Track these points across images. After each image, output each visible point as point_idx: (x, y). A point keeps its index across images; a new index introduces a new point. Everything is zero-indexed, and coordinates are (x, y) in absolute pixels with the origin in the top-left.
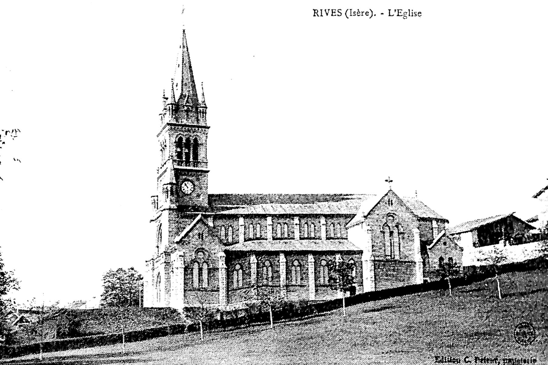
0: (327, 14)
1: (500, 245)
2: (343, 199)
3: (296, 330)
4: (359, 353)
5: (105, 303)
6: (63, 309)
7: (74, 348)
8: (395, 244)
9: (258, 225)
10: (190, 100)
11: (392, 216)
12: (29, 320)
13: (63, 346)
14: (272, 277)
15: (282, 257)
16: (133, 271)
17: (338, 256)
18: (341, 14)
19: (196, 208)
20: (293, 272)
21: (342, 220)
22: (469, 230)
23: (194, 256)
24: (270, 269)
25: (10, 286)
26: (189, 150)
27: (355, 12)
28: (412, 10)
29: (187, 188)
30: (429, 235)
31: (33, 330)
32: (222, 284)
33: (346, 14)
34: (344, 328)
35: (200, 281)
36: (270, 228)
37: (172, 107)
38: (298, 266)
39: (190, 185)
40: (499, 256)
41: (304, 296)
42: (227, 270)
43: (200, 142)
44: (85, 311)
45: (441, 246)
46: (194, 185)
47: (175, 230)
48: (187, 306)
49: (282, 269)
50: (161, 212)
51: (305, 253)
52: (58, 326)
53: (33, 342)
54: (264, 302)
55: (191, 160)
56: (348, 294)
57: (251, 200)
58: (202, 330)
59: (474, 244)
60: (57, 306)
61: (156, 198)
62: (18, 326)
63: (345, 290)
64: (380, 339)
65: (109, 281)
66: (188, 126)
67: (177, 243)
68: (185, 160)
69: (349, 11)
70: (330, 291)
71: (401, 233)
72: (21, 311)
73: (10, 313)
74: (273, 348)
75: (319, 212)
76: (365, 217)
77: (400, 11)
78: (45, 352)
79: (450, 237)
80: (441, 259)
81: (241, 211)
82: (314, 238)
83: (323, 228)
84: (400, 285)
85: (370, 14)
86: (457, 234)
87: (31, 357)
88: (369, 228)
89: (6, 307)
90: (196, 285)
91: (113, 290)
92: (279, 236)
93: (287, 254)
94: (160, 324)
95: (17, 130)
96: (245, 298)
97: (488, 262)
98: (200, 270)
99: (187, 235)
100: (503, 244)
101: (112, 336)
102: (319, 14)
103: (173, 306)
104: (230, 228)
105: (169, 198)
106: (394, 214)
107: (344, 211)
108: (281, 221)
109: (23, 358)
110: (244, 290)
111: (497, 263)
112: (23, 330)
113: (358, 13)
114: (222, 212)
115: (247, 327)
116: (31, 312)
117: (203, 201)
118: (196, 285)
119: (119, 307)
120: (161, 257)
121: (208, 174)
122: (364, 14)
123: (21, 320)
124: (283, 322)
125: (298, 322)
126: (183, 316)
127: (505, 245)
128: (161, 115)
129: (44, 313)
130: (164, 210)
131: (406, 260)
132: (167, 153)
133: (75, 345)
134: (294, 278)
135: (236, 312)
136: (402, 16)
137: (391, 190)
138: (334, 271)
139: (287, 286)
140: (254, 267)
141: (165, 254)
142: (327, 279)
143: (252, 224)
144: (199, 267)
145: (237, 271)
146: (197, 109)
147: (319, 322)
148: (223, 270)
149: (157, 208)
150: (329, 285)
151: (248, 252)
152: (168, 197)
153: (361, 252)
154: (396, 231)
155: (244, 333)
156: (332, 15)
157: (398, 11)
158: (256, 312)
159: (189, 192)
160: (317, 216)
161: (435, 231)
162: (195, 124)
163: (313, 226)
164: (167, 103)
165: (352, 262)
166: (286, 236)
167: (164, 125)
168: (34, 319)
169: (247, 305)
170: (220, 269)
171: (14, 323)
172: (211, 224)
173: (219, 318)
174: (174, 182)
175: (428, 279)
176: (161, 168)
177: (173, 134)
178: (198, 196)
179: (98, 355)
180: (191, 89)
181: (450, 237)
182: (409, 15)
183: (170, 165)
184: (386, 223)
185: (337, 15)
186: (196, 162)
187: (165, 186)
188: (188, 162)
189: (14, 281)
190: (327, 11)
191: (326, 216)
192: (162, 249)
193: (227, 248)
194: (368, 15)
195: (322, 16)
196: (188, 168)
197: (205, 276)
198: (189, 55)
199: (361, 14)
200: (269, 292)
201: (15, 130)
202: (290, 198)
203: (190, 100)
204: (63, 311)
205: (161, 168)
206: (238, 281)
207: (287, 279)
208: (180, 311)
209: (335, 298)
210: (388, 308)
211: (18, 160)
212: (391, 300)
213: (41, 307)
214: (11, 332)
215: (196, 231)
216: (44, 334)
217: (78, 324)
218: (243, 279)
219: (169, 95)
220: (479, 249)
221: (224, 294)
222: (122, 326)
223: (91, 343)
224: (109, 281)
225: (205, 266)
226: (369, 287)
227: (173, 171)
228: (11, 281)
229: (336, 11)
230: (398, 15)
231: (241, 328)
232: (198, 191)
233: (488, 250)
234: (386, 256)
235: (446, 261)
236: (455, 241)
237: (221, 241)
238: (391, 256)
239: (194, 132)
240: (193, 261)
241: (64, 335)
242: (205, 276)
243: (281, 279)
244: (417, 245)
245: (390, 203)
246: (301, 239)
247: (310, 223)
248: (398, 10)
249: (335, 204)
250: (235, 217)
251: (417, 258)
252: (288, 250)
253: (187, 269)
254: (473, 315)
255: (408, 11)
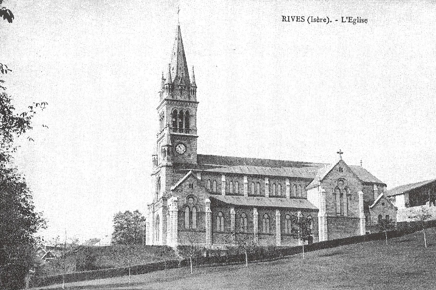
0: (293, 20)
1: (427, 206)
2: (303, 166)
3: (265, 269)
4: (315, 287)
5: (115, 241)
6: (81, 246)
7: (90, 279)
8: (345, 204)
9: (237, 183)
10: (183, 81)
11: (342, 181)
12: (54, 255)
13: (82, 278)
14: (247, 227)
15: (255, 212)
16: (138, 213)
17: (299, 213)
18: (304, 20)
19: (188, 166)
20: (264, 224)
21: (303, 183)
22: (402, 193)
23: (185, 201)
24: (246, 219)
25: (40, 226)
26: (182, 120)
27: (315, 19)
28: (360, 18)
29: (181, 149)
30: (371, 197)
31: (58, 264)
32: (207, 225)
33: (308, 20)
34: (303, 268)
35: (191, 223)
36: (246, 186)
37: (169, 87)
38: (268, 218)
39: (182, 147)
40: (425, 214)
41: (272, 243)
42: (212, 214)
43: (190, 114)
44: (99, 248)
45: (380, 206)
46: (186, 147)
47: (171, 182)
48: (180, 244)
49: (255, 221)
50: (160, 169)
51: (273, 209)
52: (77, 260)
53: (57, 274)
54: (240, 246)
55: (184, 128)
56: (307, 242)
57: (231, 162)
58: (191, 265)
59: (406, 205)
60: (76, 243)
61: (156, 157)
62: (45, 260)
63: (304, 240)
64: (332, 277)
65: (119, 222)
66: (181, 101)
67: (172, 190)
68: (179, 128)
69: (310, 18)
70: (292, 240)
71: (349, 195)
72: (48, 248)
73: (39, 249)
74: (248, 282)
75: (284, 175)
76: (320, 181)
77: (351, 18)
78: (68, 282)
79: (387, 198)
80: (380, 216)
81: (223, 170)
82: (280, 197)
83: (288, 189)
84: (348, 236)
85: (327, 20)
86: (393, 196)
87: (55, 286)
88: (324, 190)
89: (36, 244)
90: (187, 226)
91: (121, 230)
92: (253, 193)
93: (259, 208)
94: (159, 259)
95: (45, 103)
96: (226, 241)
97: (417, 219)
98: (191, 213)
99: (180, 185)
100: (429, 205)
101: (120, 269)
102: (287, 19)
103: (169, 244)
104: (215, 182)
105: (166, 157)
106: (344, 179)
107: (304, 176)
108: (255, 180)
109: (50, 287)
110: (225, 235)
111: (424, 219)
112: (50, 263)
113: (318, 20)
114: (208, 170)
115: (227, 265)
116: (55, 248)
117: (193, 160)
118: (187, 226)
119: (126, 244)
120: (160, 202)
121: (198, 138)
122: (322, 20)
123: (48, 255)
124: (255, 262)
125: (267, 263)
126: (177, 253)
127: (430, 206)
128: (160, 93)
129: (66, 250)
130: (162, 166)
131: (353, 217)
132: (165, 123)
133: (91, 277)
134: (264, 229)
135: (219, 251)
136: (352, 22)
137: (341, 160)
138: (296, 224)
139: (259, 234)
140: (233, 217)
141: (163, 199)
142: (290, 230)
143: (232, 181)
144: (190, 210)
145: (220, 217)
146: (189, 88)
147: (283, 263)
148: (209, 214)
149: (157, 166)
150: (292, 235)
151: (228, 204)
152: (165, 156)
153: (317, 211)
154: (345, 193)
155: (225, 269)
156: (297, 21)
157: (349, 19)
158: (234, 253)
159: (182, 152)
160: (284, 178)
161: (376, 194)
162: (187, 100)
163: (279, 186)
164: (165, 83)
165: (310, 217)
166: (258, 193)
167: (162, 101)
168: (58, 254)
169: (228, 248)
170: (206, 213)
171: (42, 257)
172: (199, 178)
173: (205, 255)
174: (170, 144)
175: (369, 231)
176: (160, 134)
177: (169, 108)
178: (189, 155)
179: (109, 285)
180: (184, 72)
181: (387, 198)
182: (358, 22)
183: (166, 132)
184: (337, 186)
185: (301, 21)
186: (188, 130)
187: (164, 148)
188: (181, 130)
189: (43, 220)
190: (293, 17)
191: (291, 179)
192: (161, 195)
193: (212, 196)
194: (326, 21)
195: (289, 21)
196: (182, 134)
197: (194, 219)
198: (183, 45)
199: (320, 21)
200: (245, 238)
201: (44, 103)
202: (262, 162)
203: (183, 81)
204: (81, 248)
205: (160, 134)
206: (220, 226)
207: (259, 228)
208: (175, 248)
209: (297, 245)
210: (338, 254)
211: (46, 126)
212: (340, 248)
213: (64, 244)
214: (40, 265)
215: (188, 183)
216: (66, 267)
217: (93, 259)
218: (225, 226)
219: (166, 76)
220: (409, 209)
221: (209, 235)
222: (129, 261)
223: (103, 275)
224: (119, 222)
225: (194, 211)
226: (323, 237)
227: (169, 137)
228: (41, 221)
229: (301, 18)
230: (349, 22)
231: (222, 265)
232: (189, 151)
233: (417, 208)
234: (337, 213)
235: (384, 218)
236: (392, 202)
237: (207, 190)
238: (341, 213)
239: (186, 106)
240: (185, 206)
241: (82, 268)
242: (194, 219)
243: (255, 228)
244: (361, 205)
245: (341, 170)
246: (270, 196)
247: (277, 184)
248: (349, 17)
249: (296, 169)
250: (219, 174)
251: (362, 215)
252: (260, 205)
253: (181, 213)
254: (404, 259)
255: (357, 18)
